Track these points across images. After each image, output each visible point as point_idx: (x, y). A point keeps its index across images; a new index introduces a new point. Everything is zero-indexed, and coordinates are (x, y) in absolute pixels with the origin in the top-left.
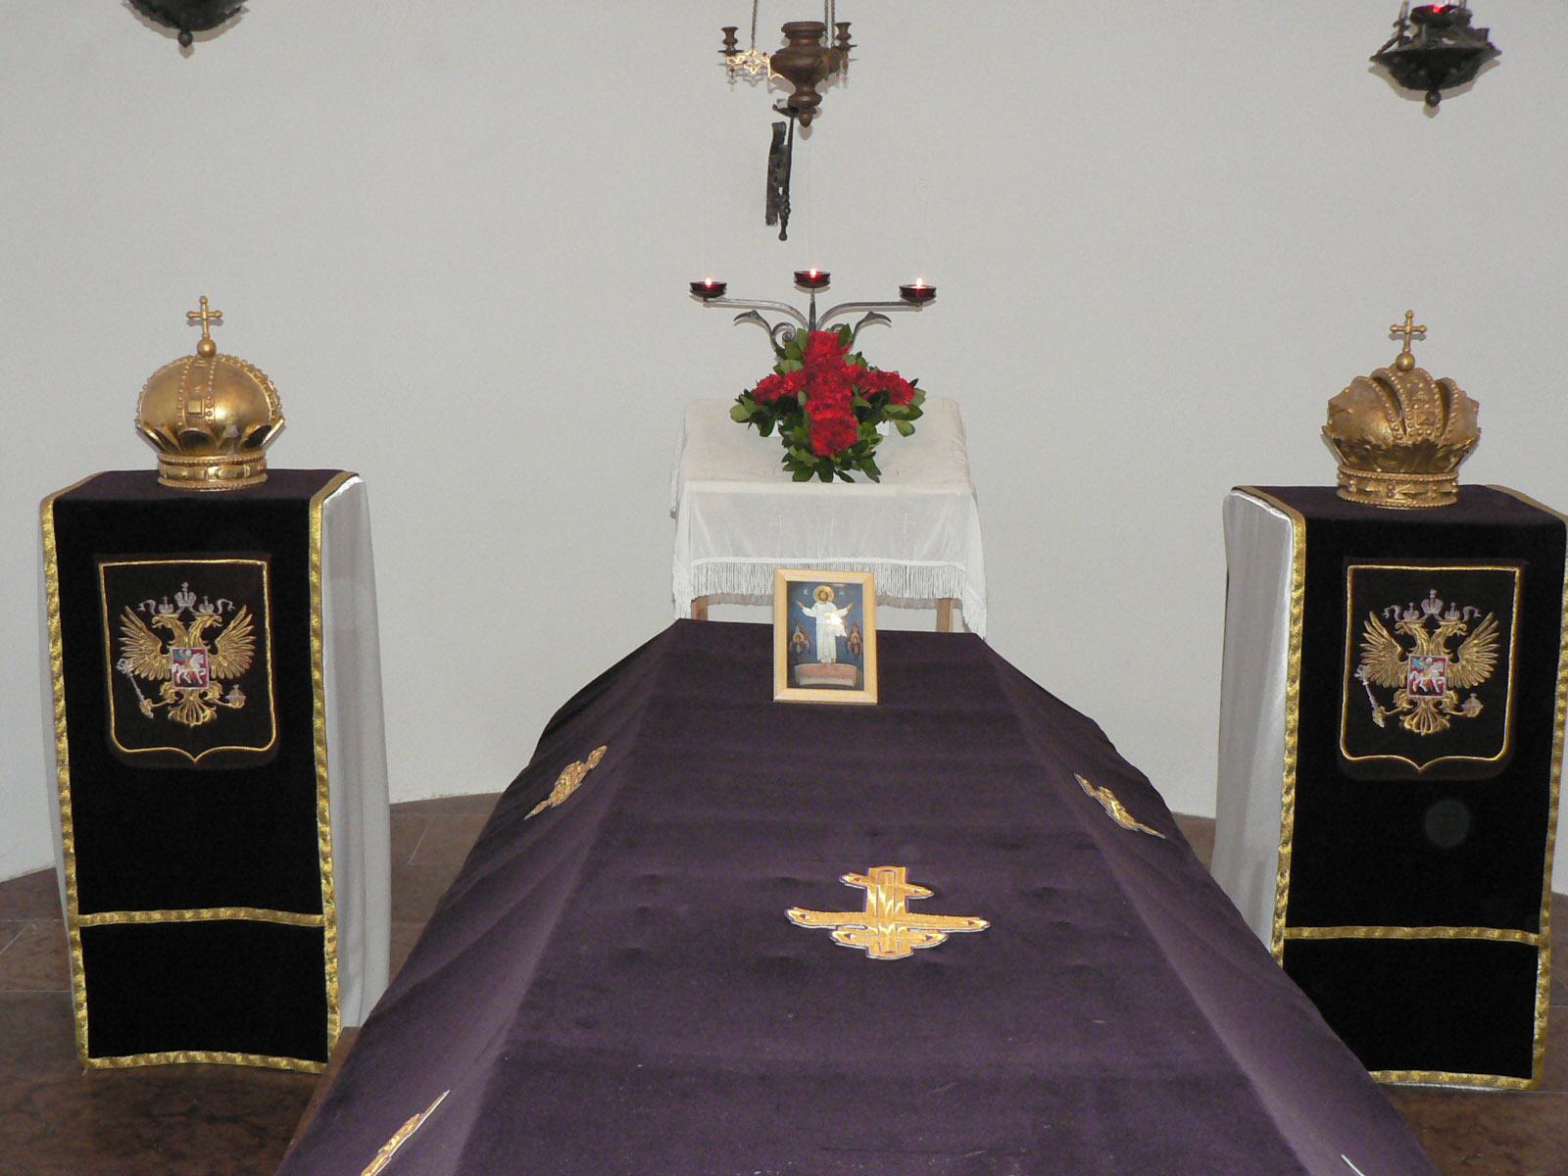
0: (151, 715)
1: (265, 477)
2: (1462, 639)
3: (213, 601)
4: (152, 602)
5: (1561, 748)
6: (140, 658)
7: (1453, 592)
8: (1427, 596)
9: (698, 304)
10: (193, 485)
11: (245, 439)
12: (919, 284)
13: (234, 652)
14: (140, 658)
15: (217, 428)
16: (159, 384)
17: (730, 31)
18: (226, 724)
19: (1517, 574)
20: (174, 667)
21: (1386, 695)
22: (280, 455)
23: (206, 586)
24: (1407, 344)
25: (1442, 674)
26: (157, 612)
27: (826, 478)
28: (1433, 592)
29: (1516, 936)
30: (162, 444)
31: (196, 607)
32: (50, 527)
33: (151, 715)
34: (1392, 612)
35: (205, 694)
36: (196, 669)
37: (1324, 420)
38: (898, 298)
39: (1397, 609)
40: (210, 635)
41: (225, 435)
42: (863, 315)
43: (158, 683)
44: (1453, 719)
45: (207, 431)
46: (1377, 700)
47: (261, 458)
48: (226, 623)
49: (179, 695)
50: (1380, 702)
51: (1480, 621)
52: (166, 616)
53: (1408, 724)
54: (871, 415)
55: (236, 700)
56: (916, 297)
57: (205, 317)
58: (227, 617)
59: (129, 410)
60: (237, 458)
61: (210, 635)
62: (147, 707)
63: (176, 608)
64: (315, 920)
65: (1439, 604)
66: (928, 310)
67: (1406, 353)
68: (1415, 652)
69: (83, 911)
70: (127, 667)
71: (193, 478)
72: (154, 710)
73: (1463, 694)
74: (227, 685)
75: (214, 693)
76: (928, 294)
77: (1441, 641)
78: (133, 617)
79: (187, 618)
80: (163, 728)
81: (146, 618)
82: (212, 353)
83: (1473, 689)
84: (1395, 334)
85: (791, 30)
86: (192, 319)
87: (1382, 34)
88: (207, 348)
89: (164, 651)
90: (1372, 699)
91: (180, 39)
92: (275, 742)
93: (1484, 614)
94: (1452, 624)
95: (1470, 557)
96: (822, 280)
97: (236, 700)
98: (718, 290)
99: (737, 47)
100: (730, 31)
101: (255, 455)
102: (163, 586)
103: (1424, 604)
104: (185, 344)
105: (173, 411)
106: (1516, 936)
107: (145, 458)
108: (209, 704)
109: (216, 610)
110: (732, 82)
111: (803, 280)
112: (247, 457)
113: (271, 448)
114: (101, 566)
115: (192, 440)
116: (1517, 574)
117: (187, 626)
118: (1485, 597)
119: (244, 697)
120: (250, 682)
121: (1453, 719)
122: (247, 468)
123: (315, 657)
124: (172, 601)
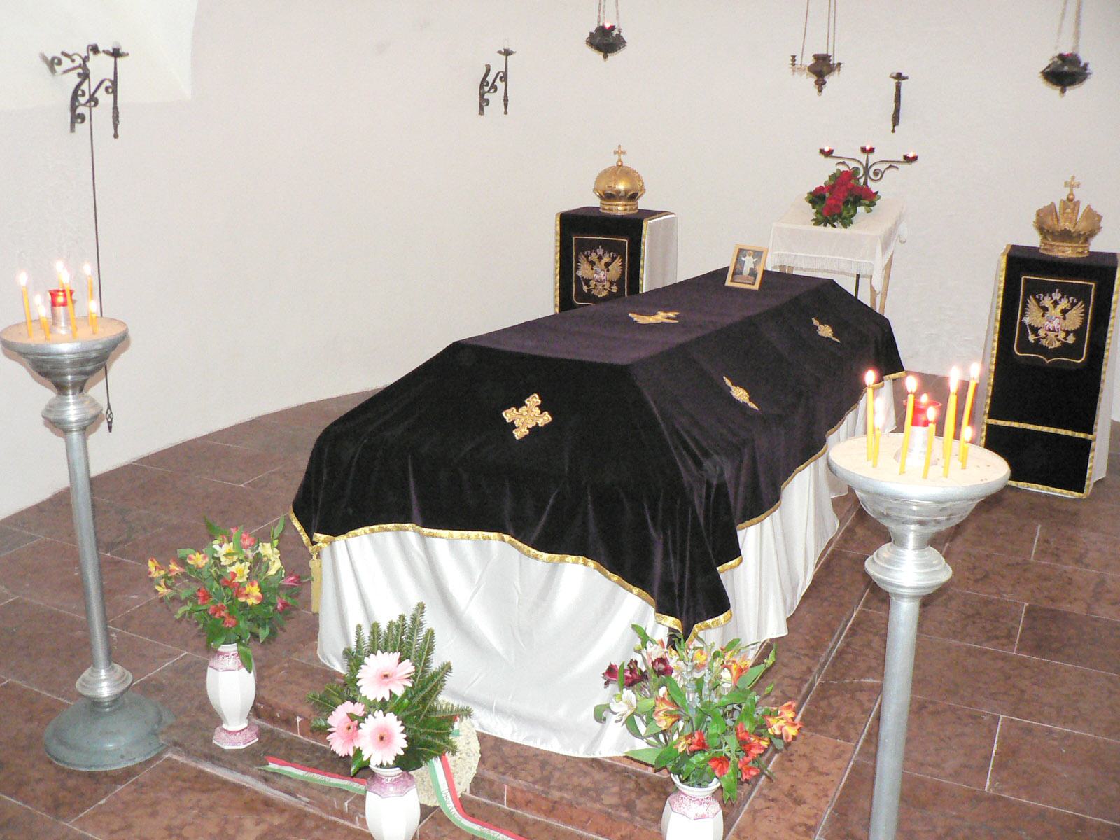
0: (1033, 342)
1: (637, 211)
2: (1068, 311)
3: (1068, 298)
4: (1042, 295)
5: (1107, 360)
6: (1032, 317)
7: (1066, 291)
8: (1055, 292)
9: (822, 157)
10: (609, 212)
11: (628, 196)
12: (911, 155)
13: (1075, 319)
14: (1032, 317)
15: (618, 192)
16: (603, 175)
17: (794, 57)
18: (1065, 349)
19: (1094, 287)
20: (595, 275)
21: (587, 282)
22: (643, 204)
23: (608, 247)
24: (1072, 190)
25: (1059, 324)
26: (1043, 299)
27: (825, 225)
28: (1057, 290)
29: (1082, 435)
30: (1042, 229)
31: (1060, 300)
32: (558, 223)
33: (1033, 342)
34: (1040, 296)
35: (1057, 336)
36: (602, 276)
37: (1034, 218)
38: (902, 160)
39: (589, 252)
40: (607, 265)
41: (620, 195)
42: (888, 165)
43: (1038, 329)
44: (1063, 343)
45: (614, 193)
46: (1031, 332)
47: (637, 204)
48: (1072, 308)
49: (1046, 335)
50: (585, 284)
51: (616, 258)
52: (1047, 302)
53: (1044, 342)
54: (856, 203)
55: (615, 289)
56: (909, 160)
57: (619, 152)
58: (613, 259)
59: (592, 185)
60: (625, 203)
61: (607, 265)
62: (585, 288)
63: (597, 254)
64: (1090, 437)
65: (1060, 295)
66: (914, 164)
67: (1072, 193)
68: (1048, 314)
69: (989, 418)
70: (1027, 320)
71: (609, 209)
72: (588, 290)
73: (1068, 333)
74: (612, 283)
75: (607, 285)
76: (915, 158)
77: (1059, 311)
78: (583, 257)
79: (600, 258)
80: (1038, 348)
81: (1038, 301)
82: (622, 165)
83: (1072, 332)
84: (1066, 185)
85: (817, 57)
86: (616, 152)
87: (1045, 62)
88: (620, 164)
89: (1043, 316)
90: (1029, 331)
91: (604, 56)
92: (1083, 362)
93: (1078, 301)
94: (1064, 304)
95: (1076, 277)
96: (872, 150)
97: (615, 289)
98: (831, 152)
99: (796, 62)
100: (794, 57)
101: (635, 203)
102: (593, 246)
103: (598, 250)
104: (612, 162)
105: (604, 186)
106: (1082, 435)
107: (595, 202)
108: (606, 290)
109: (610, 256)
110: (793, 74)
111: (864, 150)
112: (629, 203)
113: (641, 198)
114: (574, 238)
115: (608, 196)
116: (1094, 287)
117: (1055, 307)
118: (1079, 294)
119: (1074, 339)
120: (1079, 333)
121: (1063, 343)
122: (628, 207)
123: (641, 276)
124: (1051, 296)
